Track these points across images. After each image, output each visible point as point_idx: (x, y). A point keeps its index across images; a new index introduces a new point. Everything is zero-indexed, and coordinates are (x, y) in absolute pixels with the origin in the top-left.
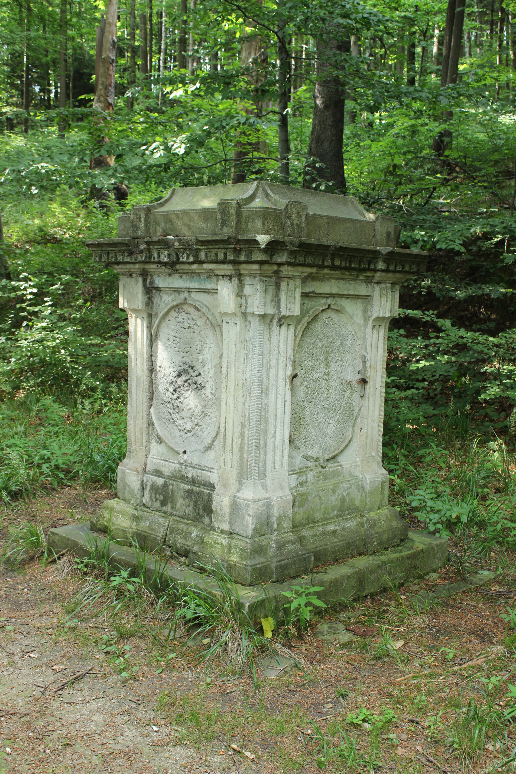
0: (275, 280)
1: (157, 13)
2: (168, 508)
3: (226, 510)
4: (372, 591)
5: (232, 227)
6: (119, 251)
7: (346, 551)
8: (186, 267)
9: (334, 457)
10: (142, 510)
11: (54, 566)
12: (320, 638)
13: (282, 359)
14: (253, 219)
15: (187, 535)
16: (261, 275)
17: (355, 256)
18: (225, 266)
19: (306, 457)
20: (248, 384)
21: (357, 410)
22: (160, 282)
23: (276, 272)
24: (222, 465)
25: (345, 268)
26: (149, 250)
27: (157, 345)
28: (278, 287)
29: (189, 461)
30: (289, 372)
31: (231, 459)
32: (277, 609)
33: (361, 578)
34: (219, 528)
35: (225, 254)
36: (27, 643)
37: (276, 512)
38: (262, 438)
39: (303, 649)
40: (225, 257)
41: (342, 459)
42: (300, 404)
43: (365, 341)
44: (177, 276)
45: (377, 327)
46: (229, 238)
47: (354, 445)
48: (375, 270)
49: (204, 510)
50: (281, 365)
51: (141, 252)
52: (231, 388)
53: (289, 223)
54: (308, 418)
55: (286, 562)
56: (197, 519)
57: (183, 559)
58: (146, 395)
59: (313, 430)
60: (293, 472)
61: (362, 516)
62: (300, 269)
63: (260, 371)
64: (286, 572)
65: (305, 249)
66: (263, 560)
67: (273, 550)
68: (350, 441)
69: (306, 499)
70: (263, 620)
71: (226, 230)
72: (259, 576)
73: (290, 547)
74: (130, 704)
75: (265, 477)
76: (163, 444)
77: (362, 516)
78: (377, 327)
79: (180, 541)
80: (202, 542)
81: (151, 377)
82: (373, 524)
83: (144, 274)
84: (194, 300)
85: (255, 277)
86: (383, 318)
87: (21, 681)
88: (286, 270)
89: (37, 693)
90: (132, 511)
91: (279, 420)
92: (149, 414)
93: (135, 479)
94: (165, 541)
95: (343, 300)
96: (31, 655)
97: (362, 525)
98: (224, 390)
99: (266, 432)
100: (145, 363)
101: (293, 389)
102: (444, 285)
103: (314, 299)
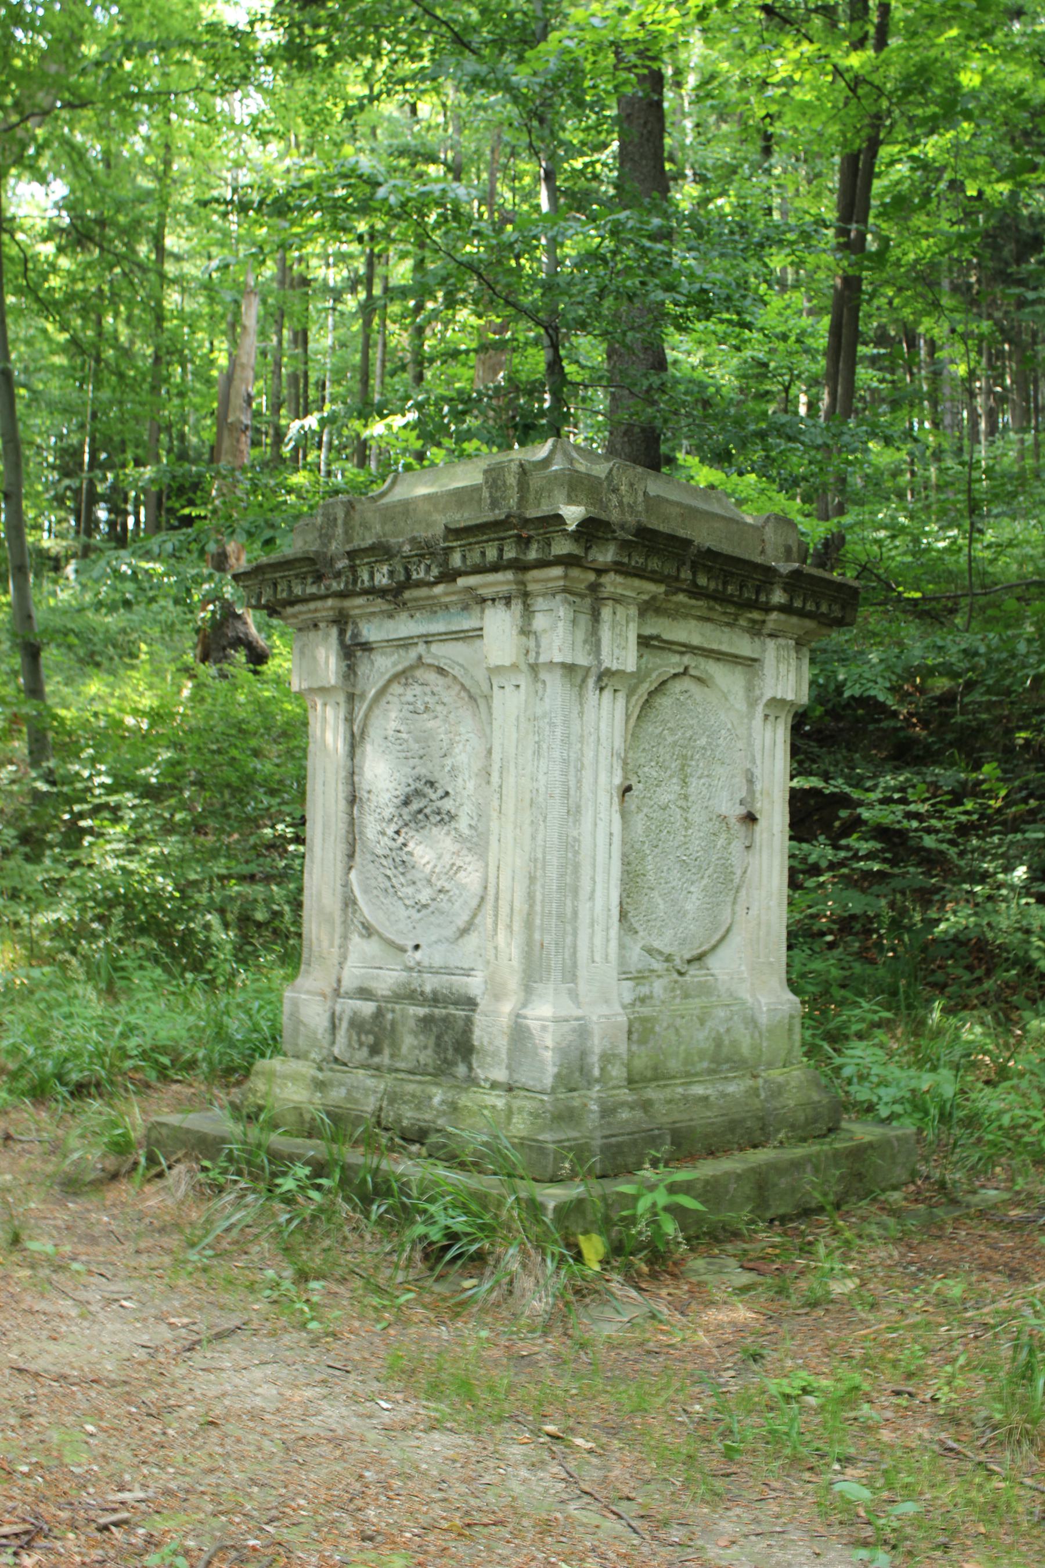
0: (592, 602)
1: (317, 383)
3: (502, 1043)
4: (782, 1211)
6: (297, 576)
7: (729, 1137)
8: (423, 592)
9: (699, 958)
10: (332, 1070)
11: (160, 1183)
12: (694, 1279)
13: (604, 753)
14: (550, 491)
15: (422, 1102)
16: (565, 590)
17: (732, 574)
18: (499, 576)
19: (650, 951)
21: (739, 872)
22: (371, 632)
24: (492, 958)
26: (353, 568)
27: (363, 753)
28: (596, 617)
29: (426, 963)
30: (617, 780)
31: (509, 949)
32: (607, 1221)
33: (761, 1183)
34: (486, 1080)
35: (501, 550)
37: (597, 1045)
38: (569, 902)
40: (500, 556)
41: (714, 962)
42: (637, 846)
43: (750, 744)
44: (404, 615)
45: (772, 718)
46: (508, 516)
47: (736, 940)
48: (767, 609)
49: (456, 1050)
50: (604, 763)
51: (338, 575)
52: (509, 807)
53: (615, 501)
55: (620, 1139)
56: (441, 1071)
57: (414, 1148)
58: (342, 848)
59: (660, 901)
60: (625, 975)
62: (637, 583)
63: (565, 773)
64: (620, 1160)
66: (575, 1134)
67: (595, 1116)
68: (728, 931)
69: (652, 1030)
70: (581, 1238)
73: (625, 1115)
75: (574, 978)
76: (375, 938)
78: (772, 718)
79: (409, 1114)
80: (454, 1107)
81: (351, 814)
82: (777, 1091)
83: (341, 620)
84: (435, 657)
85: (554, 595)
86: (783, 702)
87: (106, 1339)
88: (612, 583)
89: (140, 1355)
90: (312, 1072)
91: (600, 869)
92: (346, 884)
93: (319, 1009)
94: (379, 1123)
95: (711, 662)
96: (124, 1303)
97: (755, 1092)
99: (576, 891)
100: (341, 787)
101: (624, 814)
102: (853, 769)
103: (658, 652)
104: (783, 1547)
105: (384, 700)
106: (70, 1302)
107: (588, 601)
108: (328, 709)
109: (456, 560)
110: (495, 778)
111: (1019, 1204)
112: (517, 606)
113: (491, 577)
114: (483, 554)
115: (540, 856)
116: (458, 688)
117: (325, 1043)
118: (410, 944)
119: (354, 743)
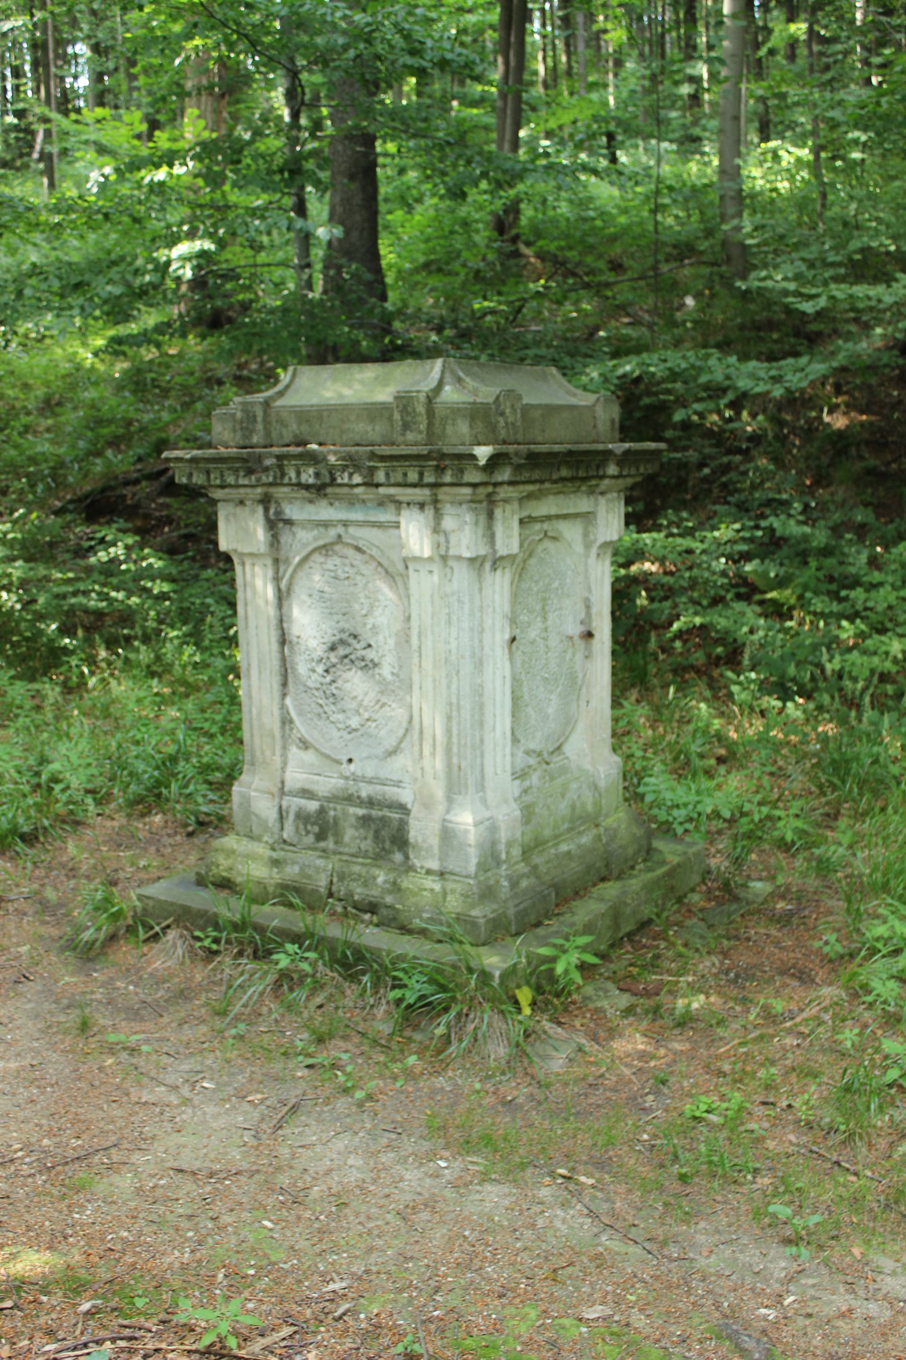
0: (487, 505)
2: (330, 844)
3: (435, 842)
5: (420, 432)
8: (346, 490)
9: (559, 748)
11: (157, 946)
15: (368, 882)
18: (417, 491)
20: (453, 658)
21: (580, 675)
22: (292, 511)
23: (489, 495)
25: (571, 479)
26: (281, 467)
28: (490, 515)
29: (359, 773)
30: (507, 636)
36: (185, 1067)
37: (503, 836)
39: (577, 1023)
41: (568, 749)
44: (324, 502)
49: (393, 842)
51: (267, 469)
52: (427, 664)
53: (502, 423)
54: (526, 697)
56: (380, 856)
57: (367, 916)
58: (276, 681)
61: (597, 826)
62: (521, 487)
65: (534, 460)
71: (410, 436)
72: (497, 931)
73: (524, 883)
74: (387, 1134)
77: (597, 826)
79: (359, 890)
81: (282, 652)
82: (613, 834)
83: (265, 501)
84: (353, 538)
85: (460, 504)
92: (283, 707)
96: (205, 1084)
97: (598, 838)
98: (416, 669)
104: (742, 1252)
105: (307, 566)
106: (163, 1088)
107: (485, 504)
108: (257, 569)
109: (380, 476)
110: (414, 641)
111: (782, 897)
112: (430, 511)
113: (410, 491)
114: (405, 475)
115: (454, 700)
116: (374, 564)
117: (276, 829)
118: (345, 759)
119: (282, 597)
